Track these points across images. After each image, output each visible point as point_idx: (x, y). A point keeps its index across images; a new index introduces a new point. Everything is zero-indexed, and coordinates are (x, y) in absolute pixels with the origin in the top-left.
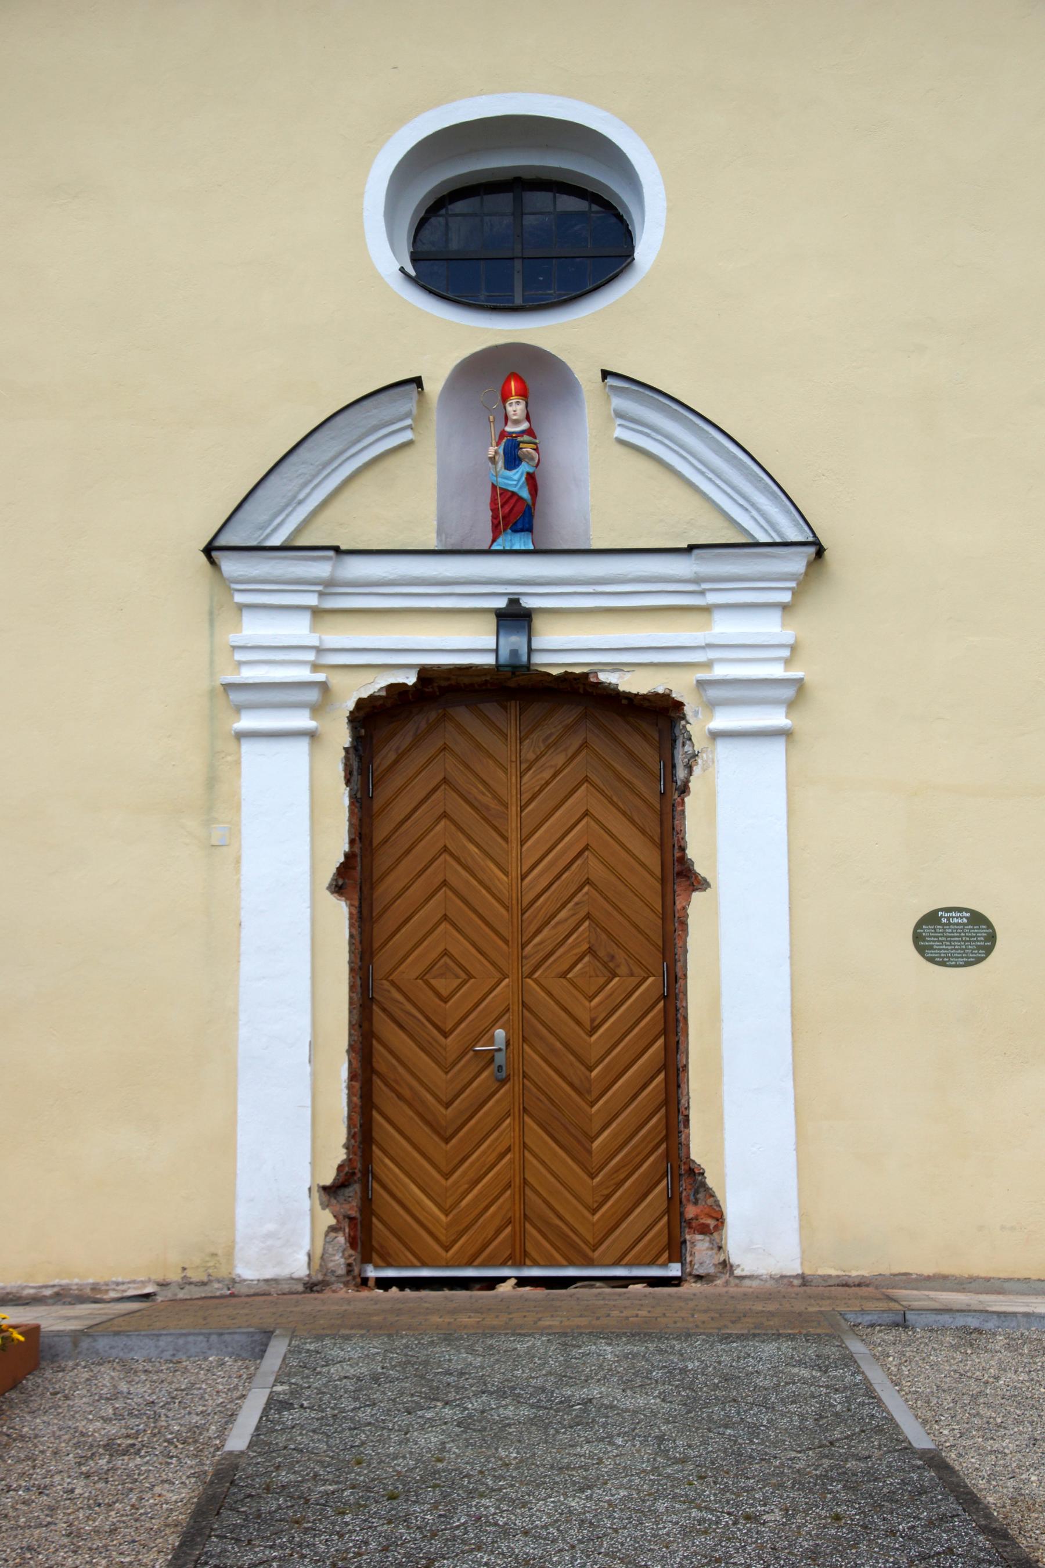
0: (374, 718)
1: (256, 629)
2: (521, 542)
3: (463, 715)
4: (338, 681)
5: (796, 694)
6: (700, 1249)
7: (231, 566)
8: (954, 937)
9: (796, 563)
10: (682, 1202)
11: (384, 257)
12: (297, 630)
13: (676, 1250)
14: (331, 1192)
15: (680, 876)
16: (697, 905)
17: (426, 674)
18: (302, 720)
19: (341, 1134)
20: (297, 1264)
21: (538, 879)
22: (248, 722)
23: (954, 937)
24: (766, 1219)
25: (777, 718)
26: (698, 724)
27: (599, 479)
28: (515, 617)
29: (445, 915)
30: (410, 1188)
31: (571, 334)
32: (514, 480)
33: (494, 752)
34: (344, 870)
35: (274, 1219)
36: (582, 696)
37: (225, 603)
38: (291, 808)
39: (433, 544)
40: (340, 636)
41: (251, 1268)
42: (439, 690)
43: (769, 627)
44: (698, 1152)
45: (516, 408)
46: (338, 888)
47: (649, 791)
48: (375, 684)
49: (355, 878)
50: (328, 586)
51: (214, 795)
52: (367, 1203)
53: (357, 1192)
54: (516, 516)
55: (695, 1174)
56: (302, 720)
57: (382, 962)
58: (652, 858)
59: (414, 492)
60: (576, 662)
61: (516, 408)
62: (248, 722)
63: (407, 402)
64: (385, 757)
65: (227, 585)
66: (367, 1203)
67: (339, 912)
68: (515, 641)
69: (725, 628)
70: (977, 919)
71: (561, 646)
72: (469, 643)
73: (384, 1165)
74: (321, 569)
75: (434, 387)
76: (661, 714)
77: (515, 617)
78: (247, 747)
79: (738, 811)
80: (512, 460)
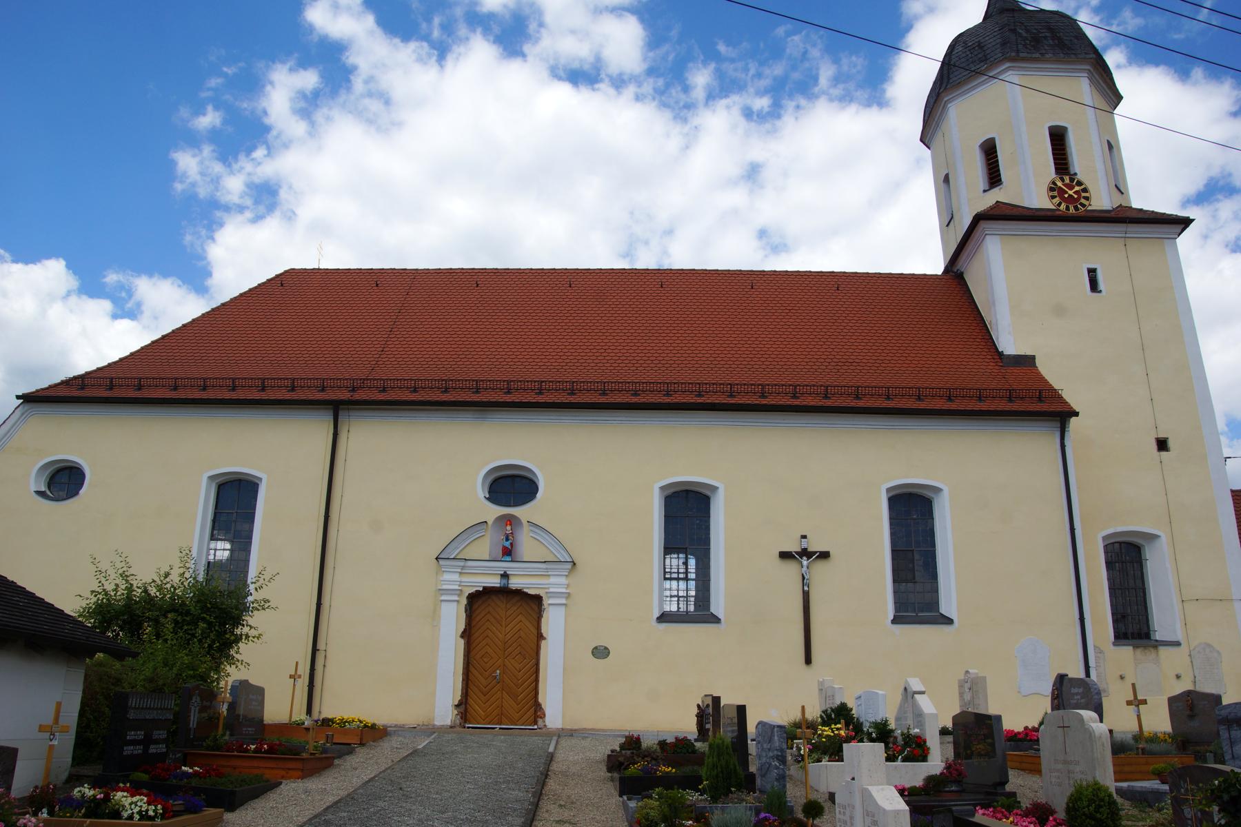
0: (473, 598)
1: (447, 577)
2: (508, 558)
3: (494, 597)
4: (465, 589)
5: (568, 596)
6: (540, 722)
7: (442, 562)
8: (601, 652)
9: (569, 566)
10: (537, 712)
11: (481, 493)
12: (456, 577)
13: (535, 723)
14: (457, 706)
15: (540, 637)
16: (543, 643)
17: (485, 588)
18: (456, 598)
19: (459, 693)
20: (448, 722)
21: (508, 636)
22: (443, 598)
23: (601, 652)
24: (555, 714)
25: (564, 601)
26: (546, 602)
27: (527, 545)
28: (505, 576)
29: (762, 234)
30: (476, 706)
31: (521, 512)
32: (507, 544)
33: (500, 607)
34: (464, 632)
35: (444, 711)
36: (519, 593)
37: (440, 571)
38: (452, 618)
39: (1058, 435)
40: (466, 579)
41: (438, 723)
42: (487, 592)
43: (563, 580)
44: (540, 700)
45: (509, 528)
46: (462, 637)
47: (536, 617)
48: (473, 590)
49: (467, 634)
50: (463, 567)
51: (435, 615)
52: (466, 710)
53: (463, 707)
54: (508, 552)
55: (539, 705)
56: (456, 598)
57: (472, 654)
58: (535, 632)
59: (484, 547)
60: (518, 587)
61: (509, 528)
62: (443, 598)
63: (484, 526)
64: (475, 606)
65: (441, 566)
66: (466, 710)
67: (462, 642)
68: (504, 581)
69: (553, 580)
70: (606, 648)
71: (515, 583)
72: (495, 582)
73: (470, 701)
74: (462, 563)
75: (490, 523)
76: (538, 599)
77: (505, 576)
78: (444, 604)
79: (553, 622)
80: (507, 539)
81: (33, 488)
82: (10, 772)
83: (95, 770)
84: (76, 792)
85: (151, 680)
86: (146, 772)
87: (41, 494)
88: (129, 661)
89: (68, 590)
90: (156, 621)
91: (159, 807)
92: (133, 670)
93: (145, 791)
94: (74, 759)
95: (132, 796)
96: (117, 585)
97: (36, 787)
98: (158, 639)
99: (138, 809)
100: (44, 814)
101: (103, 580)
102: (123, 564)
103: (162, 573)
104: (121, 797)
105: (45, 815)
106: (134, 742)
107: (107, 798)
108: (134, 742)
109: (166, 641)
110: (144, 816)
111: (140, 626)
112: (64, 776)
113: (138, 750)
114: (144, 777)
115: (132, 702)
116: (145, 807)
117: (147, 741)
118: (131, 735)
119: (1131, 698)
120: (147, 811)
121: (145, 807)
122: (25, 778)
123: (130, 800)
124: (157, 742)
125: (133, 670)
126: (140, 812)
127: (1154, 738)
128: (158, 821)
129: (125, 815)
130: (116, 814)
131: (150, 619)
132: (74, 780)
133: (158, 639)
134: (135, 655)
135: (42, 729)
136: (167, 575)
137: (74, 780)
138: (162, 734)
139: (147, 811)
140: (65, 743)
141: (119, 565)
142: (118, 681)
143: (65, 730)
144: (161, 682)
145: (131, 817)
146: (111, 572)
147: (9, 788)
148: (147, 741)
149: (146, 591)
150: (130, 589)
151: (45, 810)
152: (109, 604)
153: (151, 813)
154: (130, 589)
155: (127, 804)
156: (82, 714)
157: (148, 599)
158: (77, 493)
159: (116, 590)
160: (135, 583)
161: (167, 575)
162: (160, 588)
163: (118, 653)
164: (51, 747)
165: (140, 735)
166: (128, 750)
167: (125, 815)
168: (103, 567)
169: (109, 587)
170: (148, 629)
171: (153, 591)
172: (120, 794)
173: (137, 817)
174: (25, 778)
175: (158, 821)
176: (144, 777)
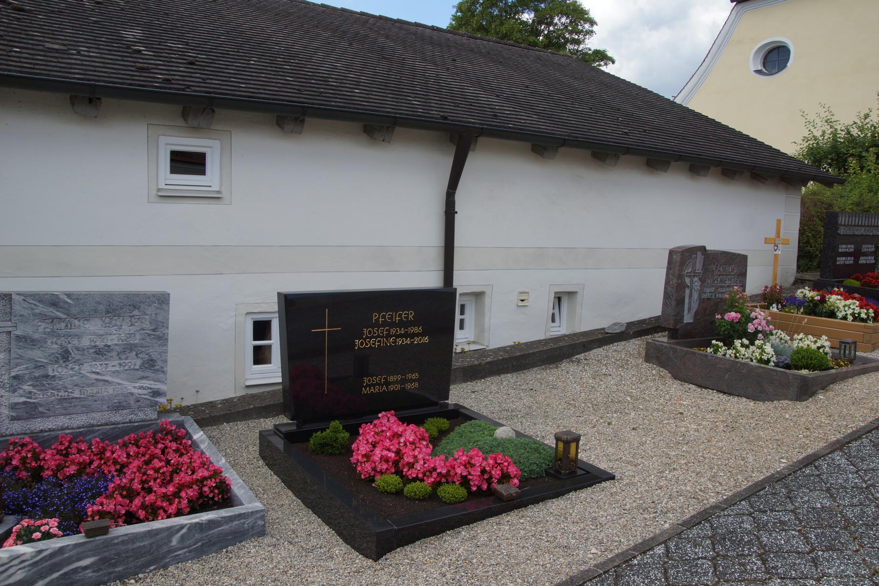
81: (753, 69)
82: (743, 274)
83: (814, 276)
84: (799, 293)
85: (858, 204)
86: (857, 279)
87: (758, 72)
88: (837, 188)
89: (788, 139)
90: (860, 157)
91: (871, 311)
92: (842, 197)
93: (856, 295)
94: (798, 267)
95: (846, 299)
96: (824, 132)
97: (766, 287)
98: (862, 170)
99: (850, 311)
100: (774, 309)
101: (812, 129)
102: (827, 113)
103: (862, 115)
104: (835, 300)
105: (775, 310)
106: (412, 381)
107: (823, 300)
108: (412, 381)
109: (869, 171)
110: (856, 318)
111: (846, 161)
112: (792, 280)
113: (850, 261)
114: (856, 284)
115: (842, 220)
116: (857, 310)
117: (857, 254)
118: (842, 248)
119: (773, 235)
120: (859, 314)
121: (857, 310)
122: (756, 281)
123: (843, 303)
124: (865, 254)
125: (842, 197)
126: (853, 314)
127: (837, 229)
128: (870, 323)
129: (840, 315)
130: (832, 314)
131: (852, 155)
132: (799, 283)
133: (862, 170)
134: (842, 182)
135: (767, 241)
136: (867, 116)
137: (799, 283)
138: (871, 248)
139: (859, 314)
140: (790, 254)
141: (823, 115)
142: (830, 205)
143: (786, 242)
144: (867, 206)
145: (845, 318)
146: (818, 121)
147: (743, 286)
148: (857, 254)
149: (848, 133)
150: (834, 134)
151: (774, 305)
152: (818, 147)
153: (863, 316)
154: (834, 134)
155: (841, 306)
156: (802, 232)
157: (852, 140)
158: (785, 66)
159: (823, 135)
160: (838, 127)
161: (867, 116)
162: (861, 129)
163: (828, 182)
164: (776, 256)
165: (851, 248)
166: (841, 260)
167: (840, 315)
168: (811, 118)
169: (818, 134)
170: (853, 162)
171: (855, 132)
172: (834, 297)
173: (850, 318)
174: (756, 281)
175: (870, 323)
176: (856, 284)
